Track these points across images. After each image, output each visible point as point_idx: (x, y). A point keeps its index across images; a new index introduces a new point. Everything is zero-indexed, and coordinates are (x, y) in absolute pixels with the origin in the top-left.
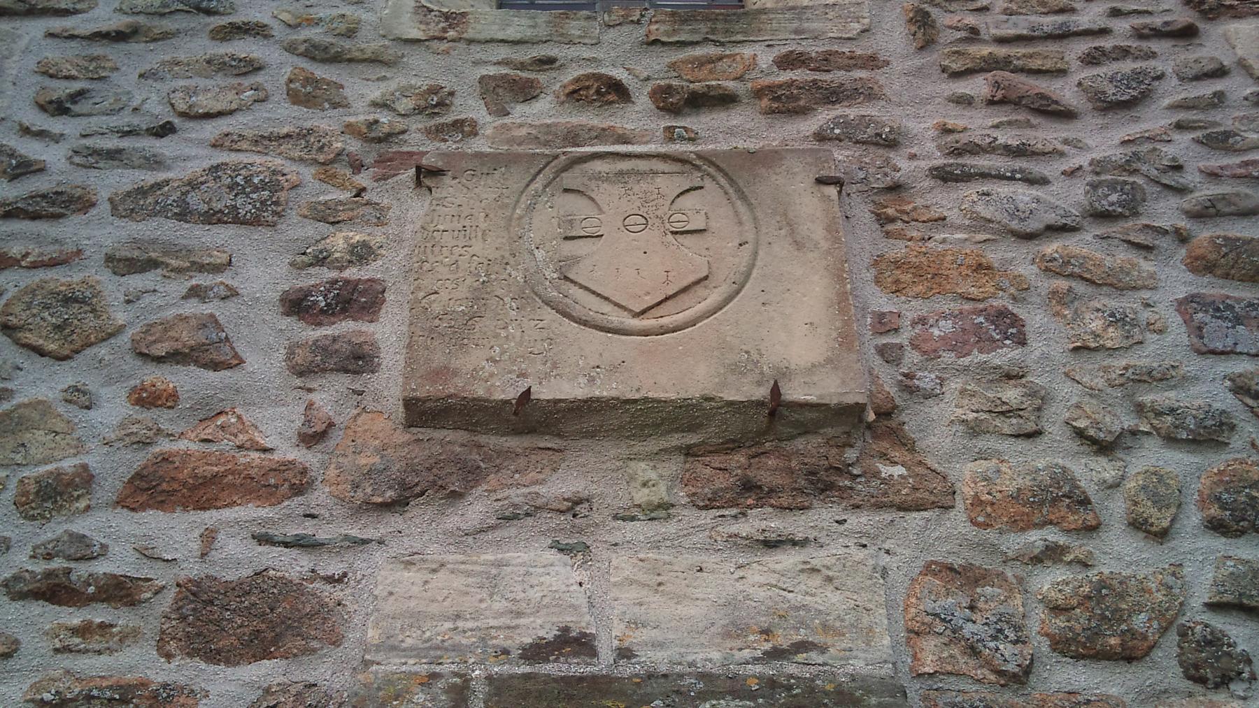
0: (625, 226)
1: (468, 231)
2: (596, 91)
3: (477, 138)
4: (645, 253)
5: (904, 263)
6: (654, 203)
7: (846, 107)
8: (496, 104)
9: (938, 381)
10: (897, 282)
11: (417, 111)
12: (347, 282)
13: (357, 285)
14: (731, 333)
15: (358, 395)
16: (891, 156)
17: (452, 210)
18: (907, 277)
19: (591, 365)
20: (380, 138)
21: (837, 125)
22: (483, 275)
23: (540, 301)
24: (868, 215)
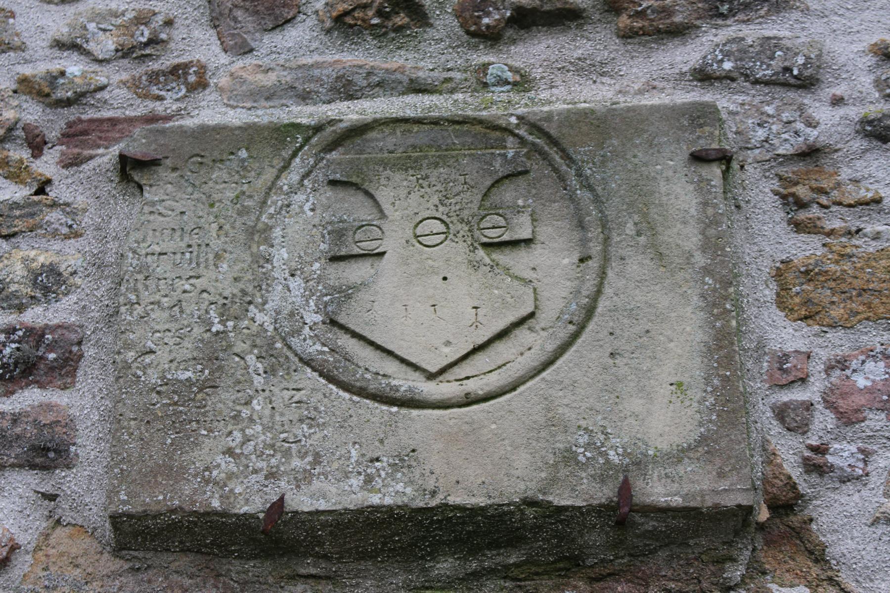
0: (416, 237)
1: (195, 253)
2: (377, 12)
3: (207, 92)
4: (445, 279)
5: (817, 274)
6: (458, 198)
7: (744, 22)
8: (233, 35)
9: (861, 456)
10: (807, 302)
11: (120, 54)
12: (30, 331)
13: (43, 335)
14: (566, 401)
15: (51, 500)
16: (806, 101)
17: (172, 221)
18: (824, 295)
19: (368, 457)
20: (68, 99)
21: (727, 55)
22: (217, 320)
23: (296, 359)
24: (770, 198)
